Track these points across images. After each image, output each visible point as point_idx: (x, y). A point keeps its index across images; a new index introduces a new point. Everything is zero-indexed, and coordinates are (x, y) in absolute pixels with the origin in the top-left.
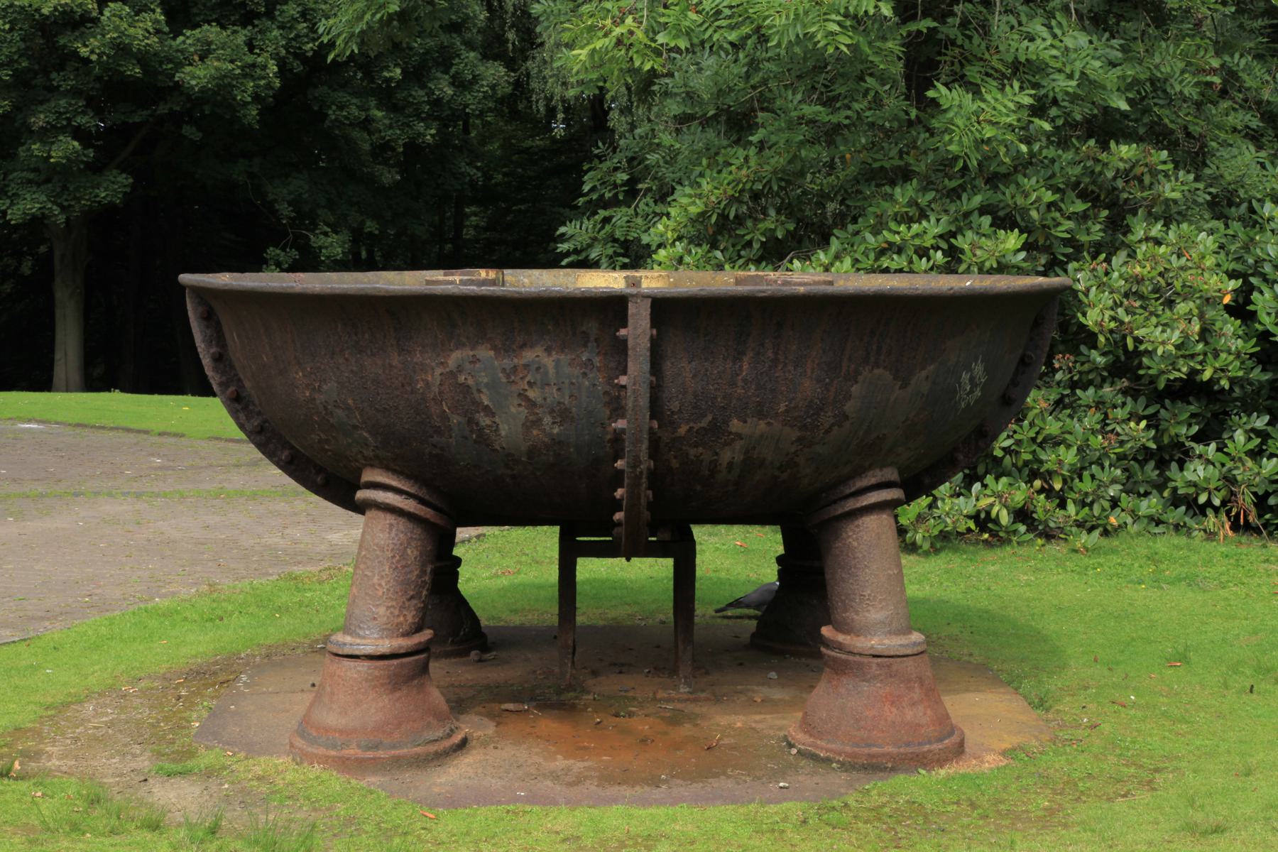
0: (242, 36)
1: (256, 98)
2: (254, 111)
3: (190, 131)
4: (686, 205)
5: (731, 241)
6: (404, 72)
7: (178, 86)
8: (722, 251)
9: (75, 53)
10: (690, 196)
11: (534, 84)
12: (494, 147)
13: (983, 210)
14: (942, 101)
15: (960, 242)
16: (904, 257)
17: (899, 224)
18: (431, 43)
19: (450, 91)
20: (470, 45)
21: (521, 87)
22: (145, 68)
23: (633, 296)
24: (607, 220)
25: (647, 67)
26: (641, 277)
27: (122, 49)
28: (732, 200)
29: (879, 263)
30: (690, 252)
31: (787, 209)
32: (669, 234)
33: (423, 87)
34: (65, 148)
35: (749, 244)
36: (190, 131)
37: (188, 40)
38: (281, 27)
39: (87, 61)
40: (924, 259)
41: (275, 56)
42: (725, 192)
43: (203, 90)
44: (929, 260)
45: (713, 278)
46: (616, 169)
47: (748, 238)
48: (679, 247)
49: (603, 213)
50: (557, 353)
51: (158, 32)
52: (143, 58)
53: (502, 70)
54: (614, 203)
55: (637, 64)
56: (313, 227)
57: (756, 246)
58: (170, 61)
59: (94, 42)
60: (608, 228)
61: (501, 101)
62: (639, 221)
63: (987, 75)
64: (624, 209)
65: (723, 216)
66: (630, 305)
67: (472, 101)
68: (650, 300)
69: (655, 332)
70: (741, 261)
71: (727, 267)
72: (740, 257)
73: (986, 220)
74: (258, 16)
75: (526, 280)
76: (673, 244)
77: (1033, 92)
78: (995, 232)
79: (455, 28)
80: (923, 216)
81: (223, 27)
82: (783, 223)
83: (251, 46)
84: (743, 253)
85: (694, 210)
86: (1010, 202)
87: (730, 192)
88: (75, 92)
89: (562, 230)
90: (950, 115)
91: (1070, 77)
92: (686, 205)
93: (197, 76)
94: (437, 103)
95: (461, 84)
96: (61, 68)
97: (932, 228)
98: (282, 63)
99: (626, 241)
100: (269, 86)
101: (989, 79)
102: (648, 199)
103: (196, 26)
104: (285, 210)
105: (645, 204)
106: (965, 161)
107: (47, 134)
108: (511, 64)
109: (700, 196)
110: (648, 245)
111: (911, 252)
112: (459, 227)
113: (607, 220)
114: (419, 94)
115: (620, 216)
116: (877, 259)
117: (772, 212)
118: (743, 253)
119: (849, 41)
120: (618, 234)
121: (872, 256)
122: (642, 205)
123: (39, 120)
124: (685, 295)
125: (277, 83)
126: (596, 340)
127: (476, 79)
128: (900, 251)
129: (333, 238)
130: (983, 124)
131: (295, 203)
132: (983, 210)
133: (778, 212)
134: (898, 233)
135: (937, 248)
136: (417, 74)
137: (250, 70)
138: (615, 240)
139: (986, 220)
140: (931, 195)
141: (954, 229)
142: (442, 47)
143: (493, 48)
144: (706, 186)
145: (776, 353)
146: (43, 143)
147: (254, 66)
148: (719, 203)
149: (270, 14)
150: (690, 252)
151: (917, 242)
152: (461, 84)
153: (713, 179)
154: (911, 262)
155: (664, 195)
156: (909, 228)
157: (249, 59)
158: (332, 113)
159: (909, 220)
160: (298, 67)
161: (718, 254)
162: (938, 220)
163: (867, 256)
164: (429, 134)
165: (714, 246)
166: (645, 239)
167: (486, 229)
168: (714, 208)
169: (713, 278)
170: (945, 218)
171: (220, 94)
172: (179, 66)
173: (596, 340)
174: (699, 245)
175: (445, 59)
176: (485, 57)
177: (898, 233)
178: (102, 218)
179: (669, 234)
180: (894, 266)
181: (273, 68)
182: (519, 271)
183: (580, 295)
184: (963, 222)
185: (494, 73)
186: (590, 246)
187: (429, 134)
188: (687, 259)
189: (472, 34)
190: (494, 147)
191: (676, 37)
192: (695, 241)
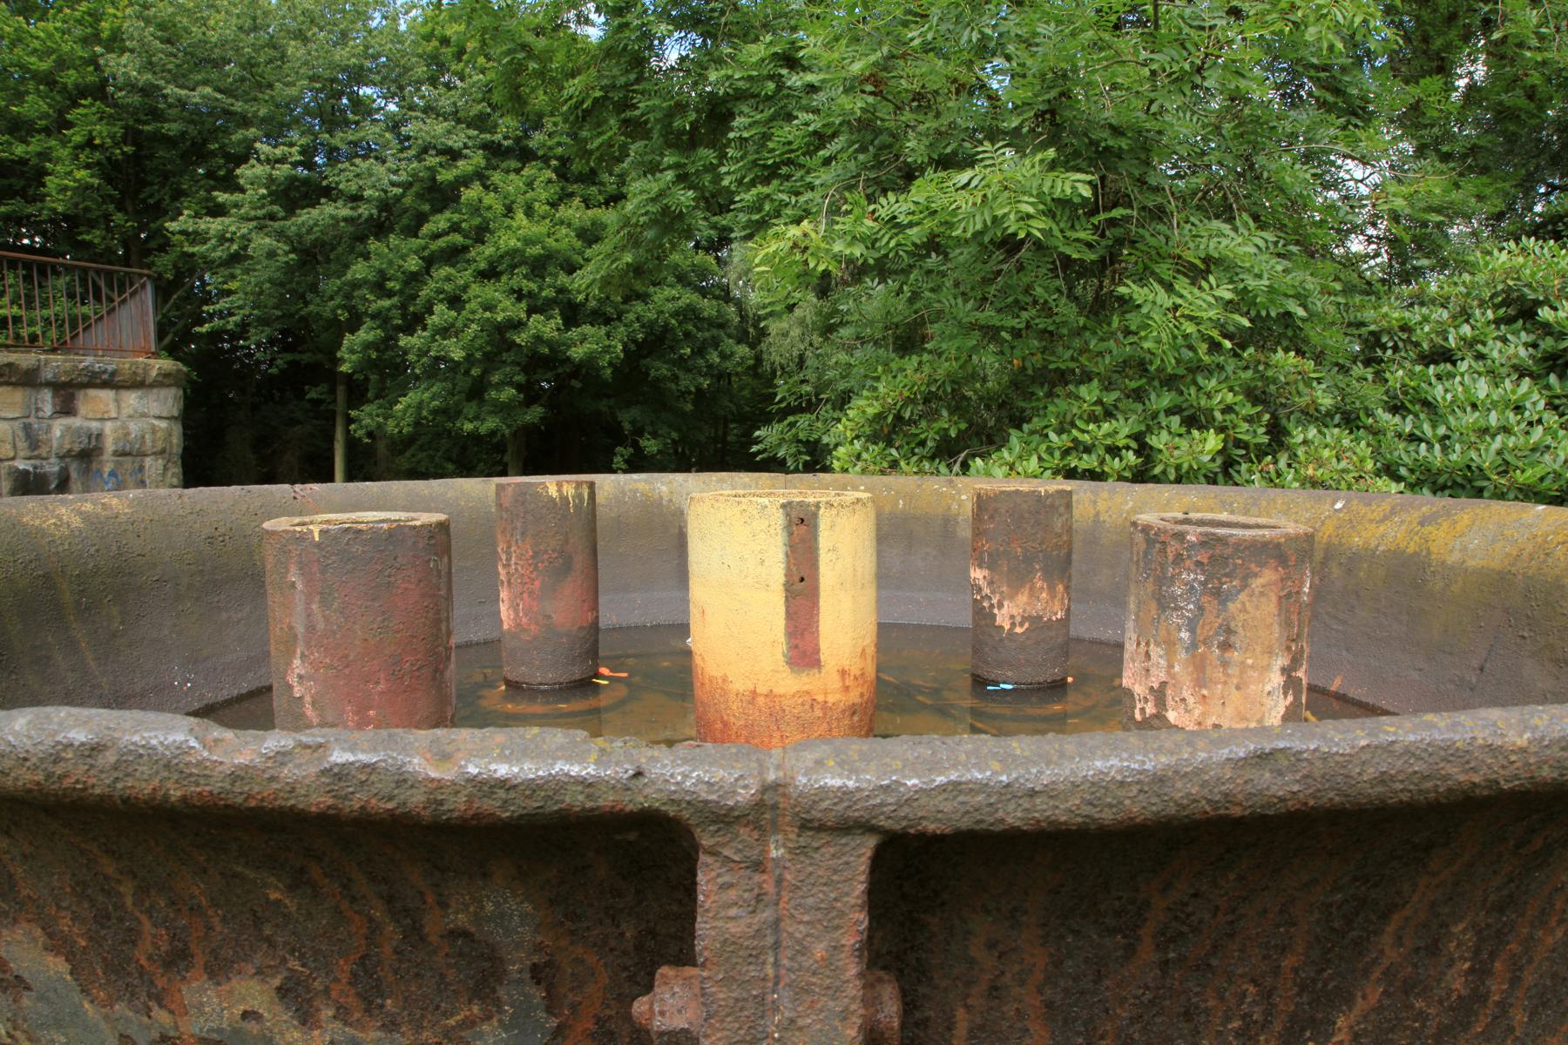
0: (603, 330)
1: (610, 364)
2: (609, 371)
3: (576, 384)
4: (863, 408)
5: (905, 439)
6: (692, 350)
7: (568, 359)
8: (897, 449)
9: (514, 341)
10: (867, 398)
11: (765, 356)
12: (746, 393)
13: (1169, 412)
14: (1135, 297)
15: (1153, 441)
16: (1094, 456)
17: (1088, 422)
18: (707, 334)
19: (718, 360)
20: (730, 336)
21: (758, 359)
22: (551, 349)
23: (725, 818)
24: (792, 425)
25: (821, 268)
26: (817, 506)
27: (538, 338)
28: (909, 401)
29: (1065, 462)
30: (867, 450)
31: (959, 406)
32: (848, 433)
33: (703, 357)
34: (509, 393)
35: (922, 443)
36: (576, 384)
37: (574, 333)
38: (625, 325)
39: (520, 346)
40: (1117, 460)
41: (621, 341)
42: (901, 394)
43: (581, 360)
44: (1121, 460)
45: (919, 486)
46: (803, 382)
47: (923, 436)
48: (857, 445)
49: (791, 419)
50: (342, 1014)
51: (558, 329)
52: (549, 343)
53: (747, 349)
54: (799, 410)
55: (812, 265)
56: (641, 435)
57: (930, 444)
58: (564, 344)
59: (524, 335)
60: (794, 430)
61: (749, 368)
62: (819, 424)
63: (1178, 271)
64: (808, 415)
65: (899, 418)
66: (708, 879)
67: (729, 365)
68: (871, 842)
69: (890, 1011)
70: (915, 458)
71: (902, 463)
72: (914, 454)
73: (1175, 421)
74: (613, 320)
75: (664, 489)
76: (852, 443)
77: (1231, 287)
78: (1189, 432)
79: (721, 326)
80: (1109, 414)
81: (593, 326)
82: (956, 423)
83: (608, 335)
84: (916, 450)
85: (871, 411)
86: (1195, 404)
87: (906, 394)
88: (514, 363)
89: (757, 433)
90: (1144, 310)
91: (1259, 276)
92: (863, 408)
93: (577, 353)
94: (710, 367)
95: (724, 356)
96: (508, 350)
97: (1121, 429)
98: (625, 346)
99: (808, 441)
100: (618, 357)
101: (1180, 277)
102: (829, 406)
103: (578, 326)
104: (627, 426)
105: (825, 411)
106: (1162, 360)
107: (499, 386)
108: (752, 346)
109: (877, 399)
110: (828, 444)
111: (1101, 452)
112: (725, 434)
113: (792, 425)
114: (701, 362)
115: (803, 420)
116: (1062, 458)
117: (945, 413)
118: (916, 450)
119: (1042, 226)
120: (802, 436)
121: (1057, 454)
122: (822, 413)
123: (495, 378)
124: (1138, 807)
125: (622, 355)
126: (537, 974)
127: (732, 354)
128: (1088, 450)
129: (653, 441)
130: (1182, 320)
131: (633, 422)
132: (1169, 412)
133: (951, 414)
134: (1088, 432)
135: (1128, 448)
136: (700, 352)
137: (606, 350)
138: (799, 441)
139: (1175, 421)
140: (1115, 395)
141: (1143, 428)
142: (713, 337)
143: (742, 338)
144: (882, 388)
145: (1480, 972)
146: (497, 390)
147: (609, 346)
148: (895, 404)
149: (619, 318)
150: (867, 450)
151: (1109, 441)
152: (724, 356)
153: (888, 383)
154: (1102, 462)
155: (843, 400)
156: (1099, 427)
157: (607, 343)
158: (653, 373)
159: (1093, 418)
160: (633, 347)
161: (894, 452)
162: (1127, 420)
163: (1051, 454)
164: (706, 383)
165: (890, 444)
166: (825, 440)
167: (742, 436)
168: (890, 410)
169: (919, 486)
170: (1133, 418)
171: (590, 362)
172: (569, 347)
173: (537, 974)
174: (875, 443)
175: (716, 343)
176: (739, 342)
177: (1088, 432)
178: (528, 431)
179: (848, 433)
180: (1083, 465)
181: (620, 347)
182: (656, 475)
183: (318, 801)
184: (1152, 422)
185: (743, 350)
186: (780, 445)
187: (706, 383)
188: (865, 456)
189: (732, 330)
190: (746, 393)
191: (850, 244)
192: (873, 438)
